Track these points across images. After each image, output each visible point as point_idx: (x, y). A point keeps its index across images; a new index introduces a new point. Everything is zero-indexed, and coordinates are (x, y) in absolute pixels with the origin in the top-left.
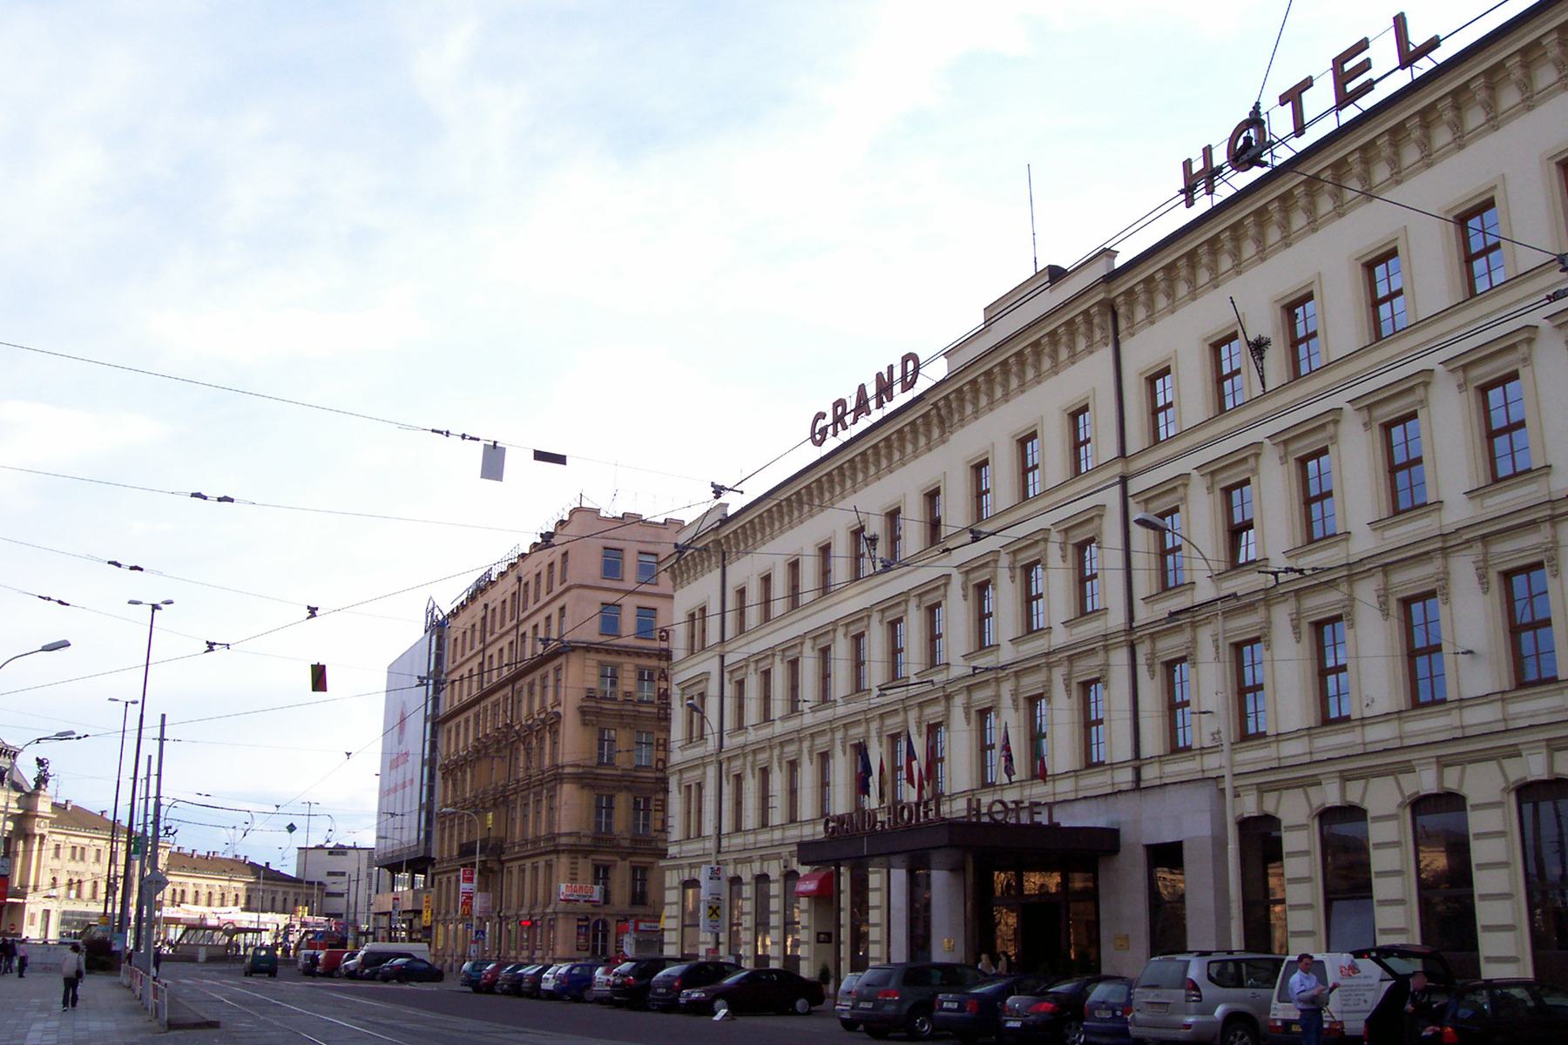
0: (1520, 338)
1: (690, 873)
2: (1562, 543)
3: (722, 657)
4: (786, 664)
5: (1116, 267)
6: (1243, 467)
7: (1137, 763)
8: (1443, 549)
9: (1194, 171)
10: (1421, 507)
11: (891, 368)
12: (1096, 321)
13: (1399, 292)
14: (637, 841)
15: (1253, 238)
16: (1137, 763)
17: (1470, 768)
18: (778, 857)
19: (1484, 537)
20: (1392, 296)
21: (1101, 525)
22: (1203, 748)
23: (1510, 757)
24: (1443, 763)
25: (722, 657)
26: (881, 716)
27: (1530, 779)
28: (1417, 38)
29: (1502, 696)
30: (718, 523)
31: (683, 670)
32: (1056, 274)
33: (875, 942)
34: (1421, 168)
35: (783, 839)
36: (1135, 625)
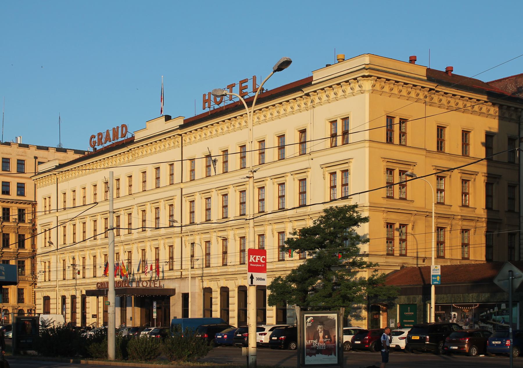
11: (118, 127)
30: (55, 167)
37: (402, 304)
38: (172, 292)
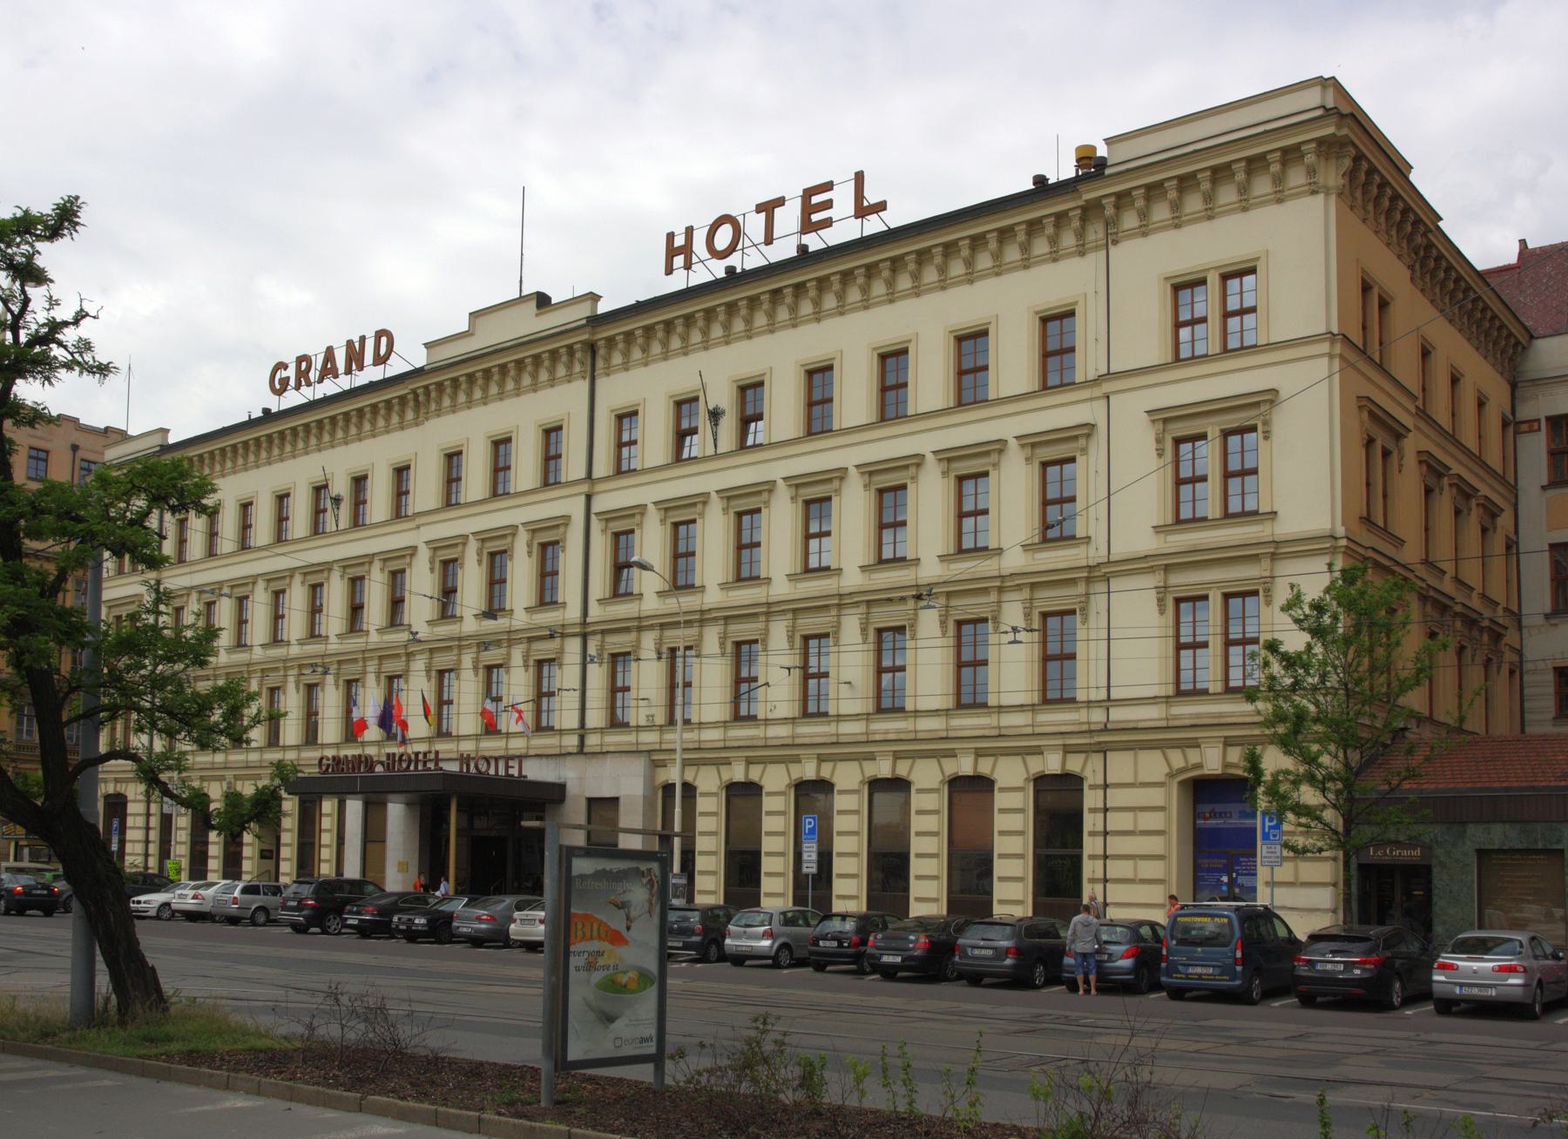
0: (1266, 398)
1: (115, 787)
2: (566, 650)
3: (589, 498)
4: (307, 587)
5: (599, 312)
6: (692, 510)
7: (582, 732)
8: (1273, 554)
9: (676, 245)
10: (689, 587)
11: (363, 339)
12: (578, 355)
13: (1253, 310)
14: (20, 747)
15: (765, 312)
16: (582, 732)
17: (703, 768)
18: (221, 779)
19: (662, 625)
20: (1242, 312)
21: (565, 532)
22: (638, 726)
23: (794, 762)
24: (979, 754)
25: (589, 498)
26: (380, 658)
27: (879, 777)
28: (871, 197)
29: (867, 717)
31: (605, 491)
32: (542, 300)
33: (248, 858)
34: (859, 307)
35: (226, 763)
36: (588, 620)
37: (1496, 847)
38: (554, 794)
